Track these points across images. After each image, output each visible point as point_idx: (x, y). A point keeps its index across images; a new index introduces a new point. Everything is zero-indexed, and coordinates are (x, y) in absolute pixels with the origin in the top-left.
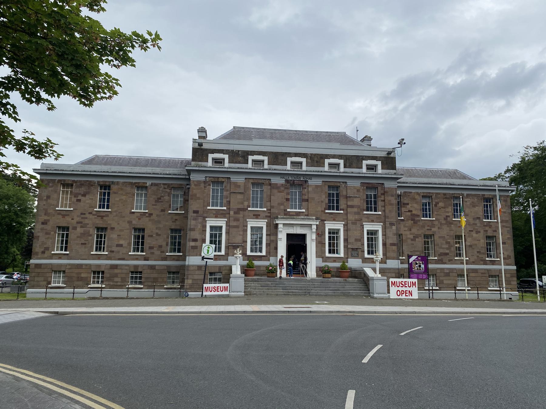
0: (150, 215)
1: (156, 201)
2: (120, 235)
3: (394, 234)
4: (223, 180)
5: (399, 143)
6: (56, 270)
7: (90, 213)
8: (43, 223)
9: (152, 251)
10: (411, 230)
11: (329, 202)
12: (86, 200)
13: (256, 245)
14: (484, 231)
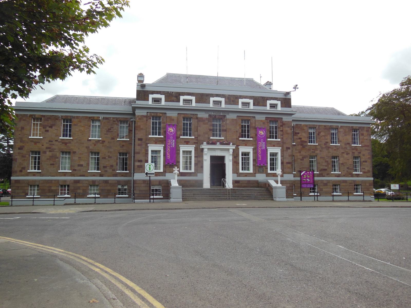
0: (103, 142)
1: (107, 131)
2: (80, 158)
3: (290, 156)
4: (161, 115)
5: (294, 88)
6: (31, 184)
7: (56, 141)
8: (19, 149)
9: (106, 169)
10: (300, 153)
11: (242, 132)
12: (52, 131)
13: (187, 165)
14: (352, 153)
